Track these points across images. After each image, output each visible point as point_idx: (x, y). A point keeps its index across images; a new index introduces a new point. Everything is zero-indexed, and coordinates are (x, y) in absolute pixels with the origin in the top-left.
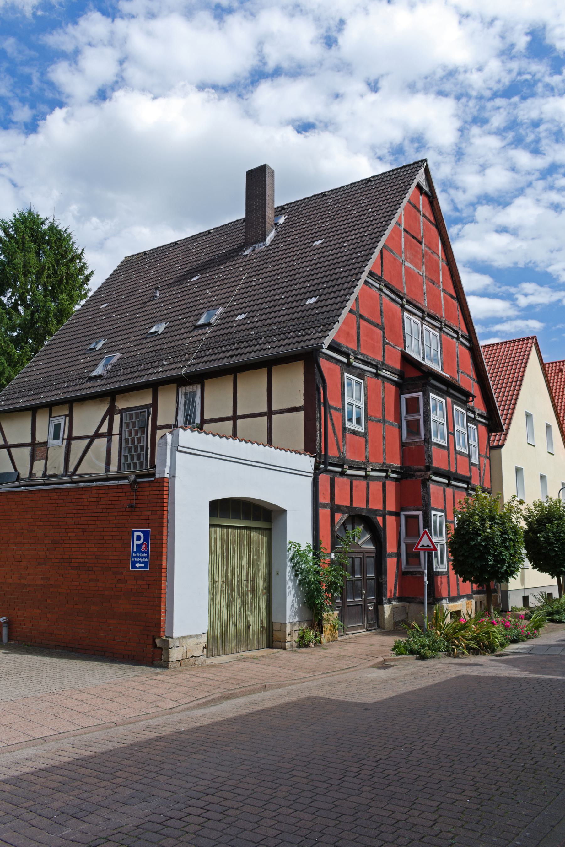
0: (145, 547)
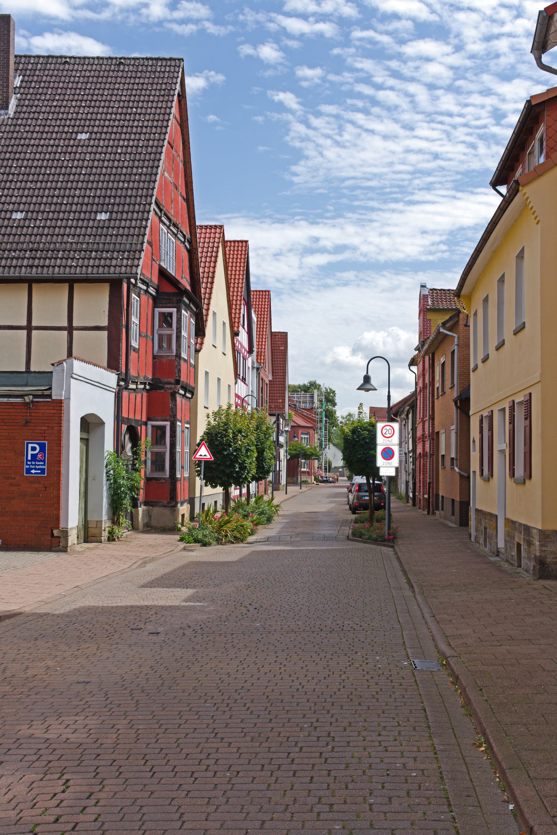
0: (42, 456)
